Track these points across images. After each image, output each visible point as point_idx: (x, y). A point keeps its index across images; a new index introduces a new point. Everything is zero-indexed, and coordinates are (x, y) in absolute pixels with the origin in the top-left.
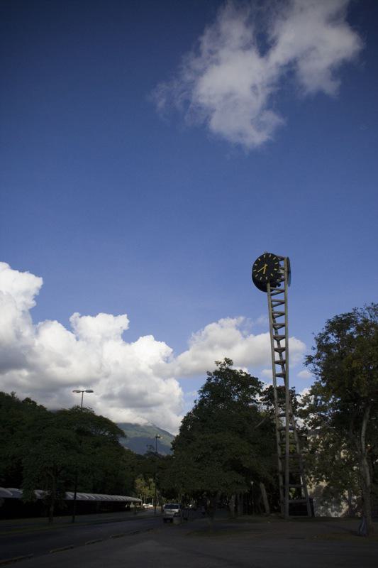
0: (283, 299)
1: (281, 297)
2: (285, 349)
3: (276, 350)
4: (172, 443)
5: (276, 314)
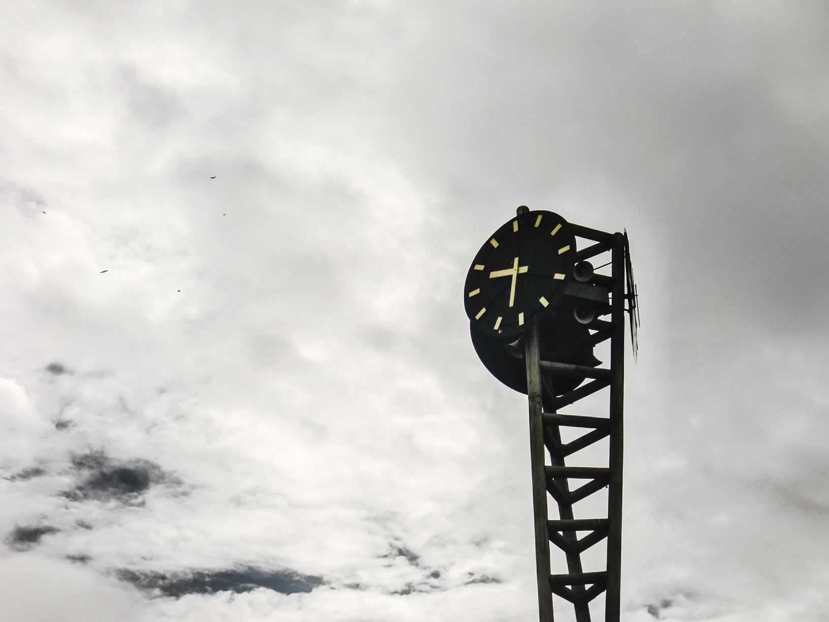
1: (596, 405)
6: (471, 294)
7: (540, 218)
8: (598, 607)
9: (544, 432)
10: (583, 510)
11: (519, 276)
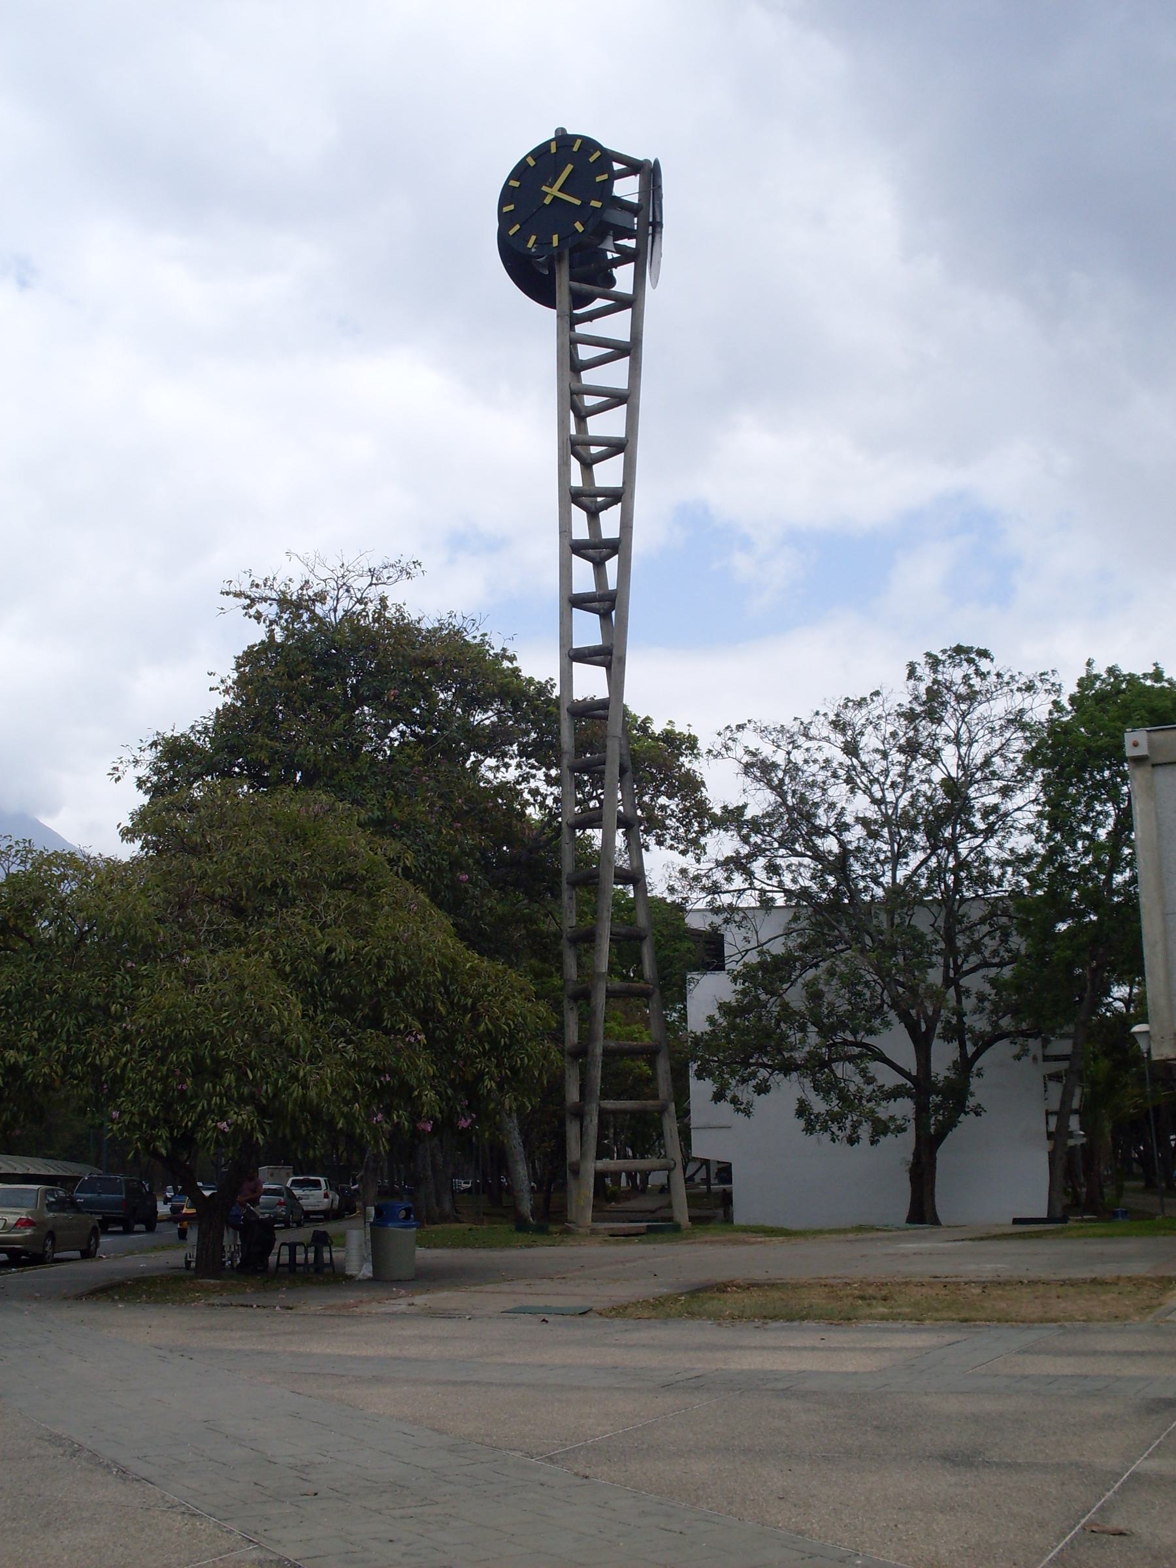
0: (625, 336)
1: (616, 326)
2: (618, 547)
3: (578, 548)
4: (725, 808)
5: (594, 450)
6: (506, 209)
7: (579, 142)
8: (612, 565)
9: (569, 343)
10: (598, 426)
11: (551, 186)
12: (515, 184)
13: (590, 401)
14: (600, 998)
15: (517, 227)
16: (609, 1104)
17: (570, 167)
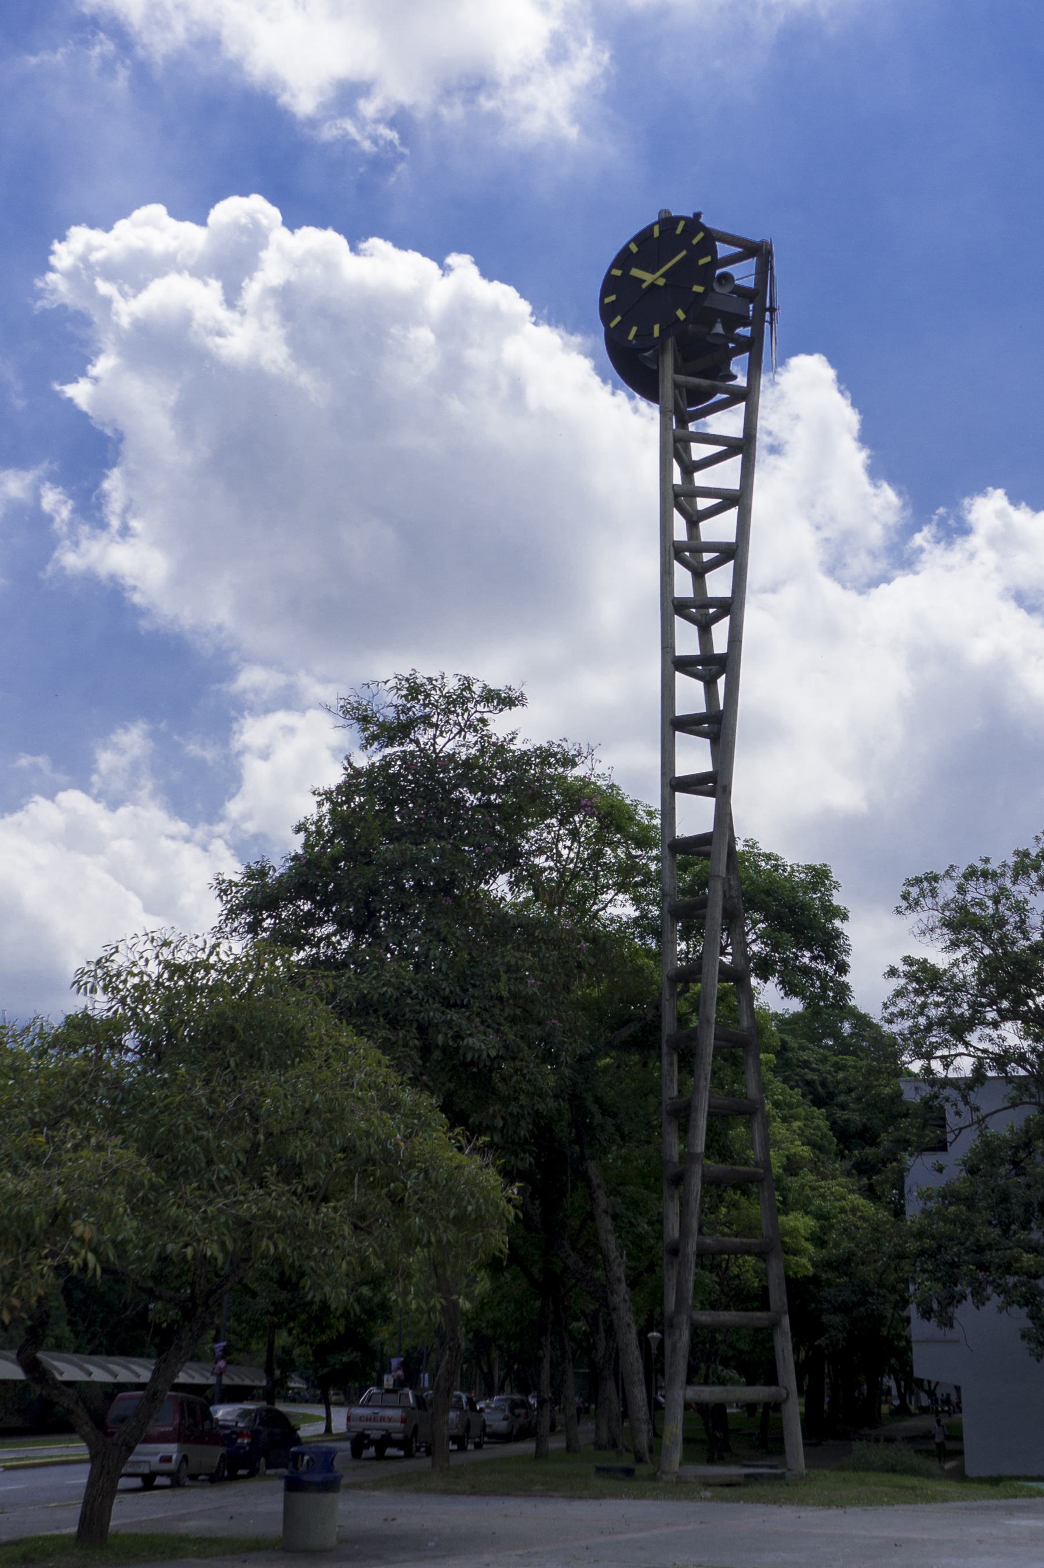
3: (685, 665)
5: (707, 557)
6: (607, 300)
7: (682, 224)
12: (617, 272)
13: (703, 503)
14: (696, 1184)
15: (619, 318)
16: (705, 1317)
17: (684, 253)
